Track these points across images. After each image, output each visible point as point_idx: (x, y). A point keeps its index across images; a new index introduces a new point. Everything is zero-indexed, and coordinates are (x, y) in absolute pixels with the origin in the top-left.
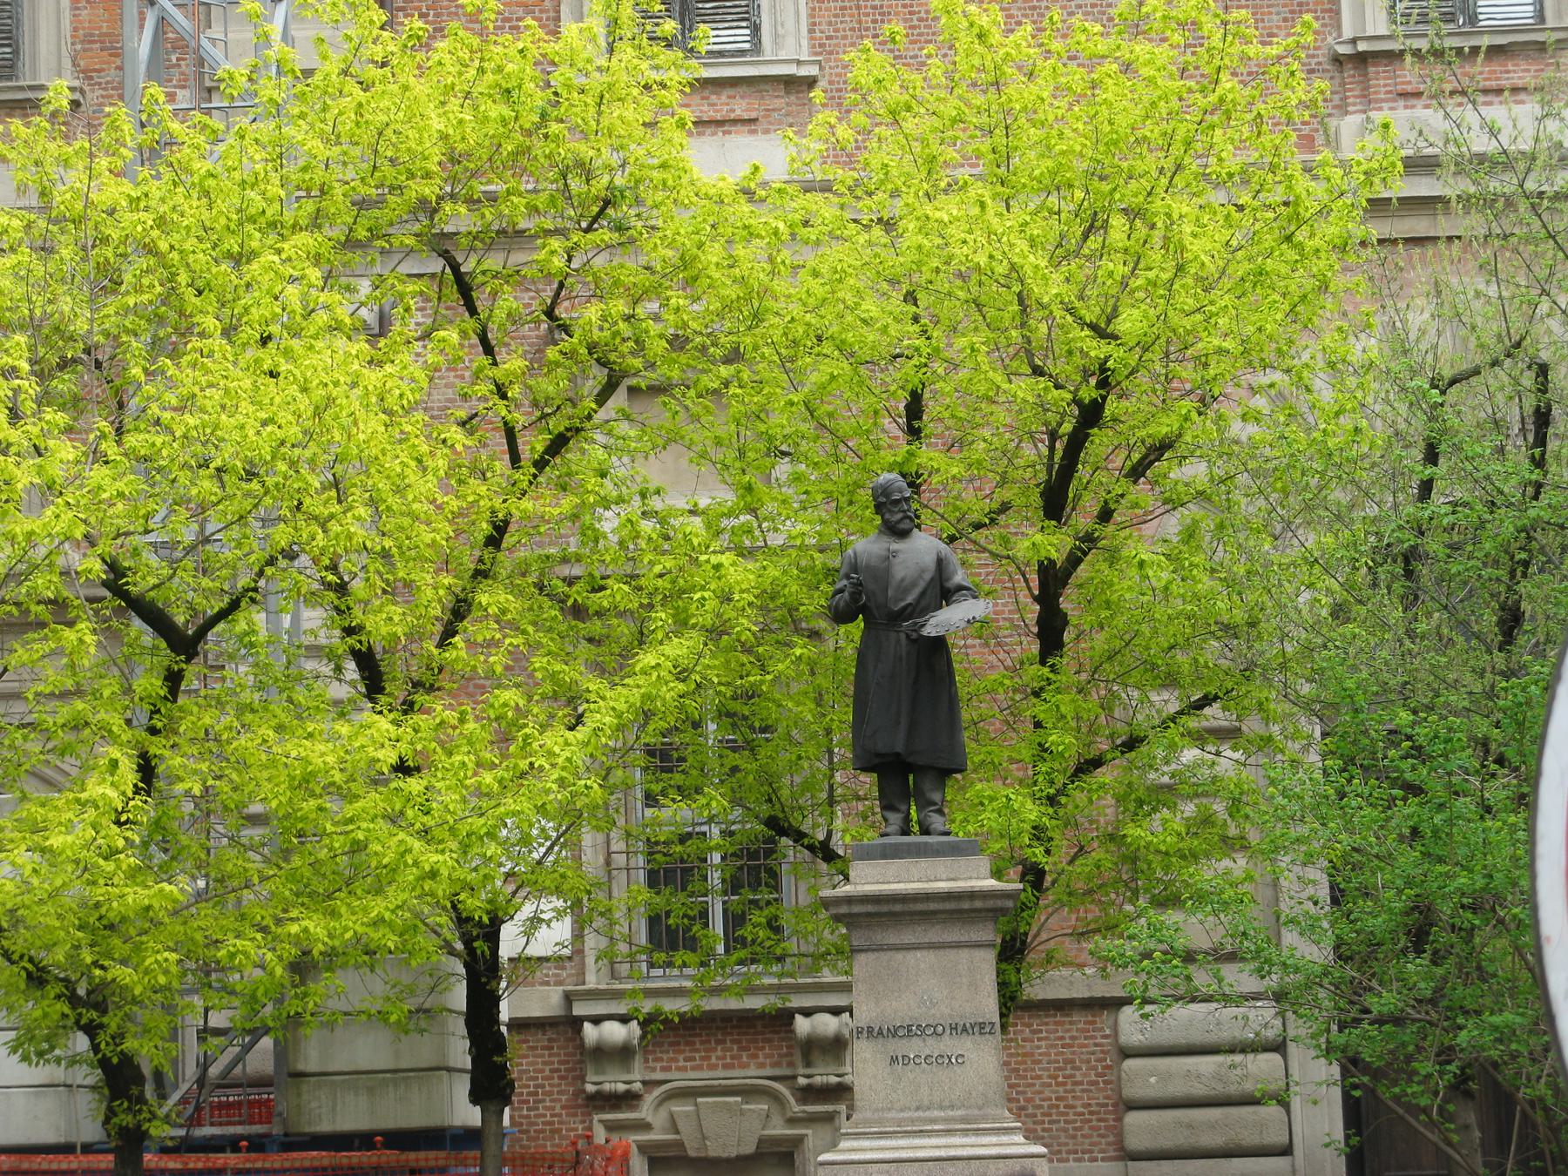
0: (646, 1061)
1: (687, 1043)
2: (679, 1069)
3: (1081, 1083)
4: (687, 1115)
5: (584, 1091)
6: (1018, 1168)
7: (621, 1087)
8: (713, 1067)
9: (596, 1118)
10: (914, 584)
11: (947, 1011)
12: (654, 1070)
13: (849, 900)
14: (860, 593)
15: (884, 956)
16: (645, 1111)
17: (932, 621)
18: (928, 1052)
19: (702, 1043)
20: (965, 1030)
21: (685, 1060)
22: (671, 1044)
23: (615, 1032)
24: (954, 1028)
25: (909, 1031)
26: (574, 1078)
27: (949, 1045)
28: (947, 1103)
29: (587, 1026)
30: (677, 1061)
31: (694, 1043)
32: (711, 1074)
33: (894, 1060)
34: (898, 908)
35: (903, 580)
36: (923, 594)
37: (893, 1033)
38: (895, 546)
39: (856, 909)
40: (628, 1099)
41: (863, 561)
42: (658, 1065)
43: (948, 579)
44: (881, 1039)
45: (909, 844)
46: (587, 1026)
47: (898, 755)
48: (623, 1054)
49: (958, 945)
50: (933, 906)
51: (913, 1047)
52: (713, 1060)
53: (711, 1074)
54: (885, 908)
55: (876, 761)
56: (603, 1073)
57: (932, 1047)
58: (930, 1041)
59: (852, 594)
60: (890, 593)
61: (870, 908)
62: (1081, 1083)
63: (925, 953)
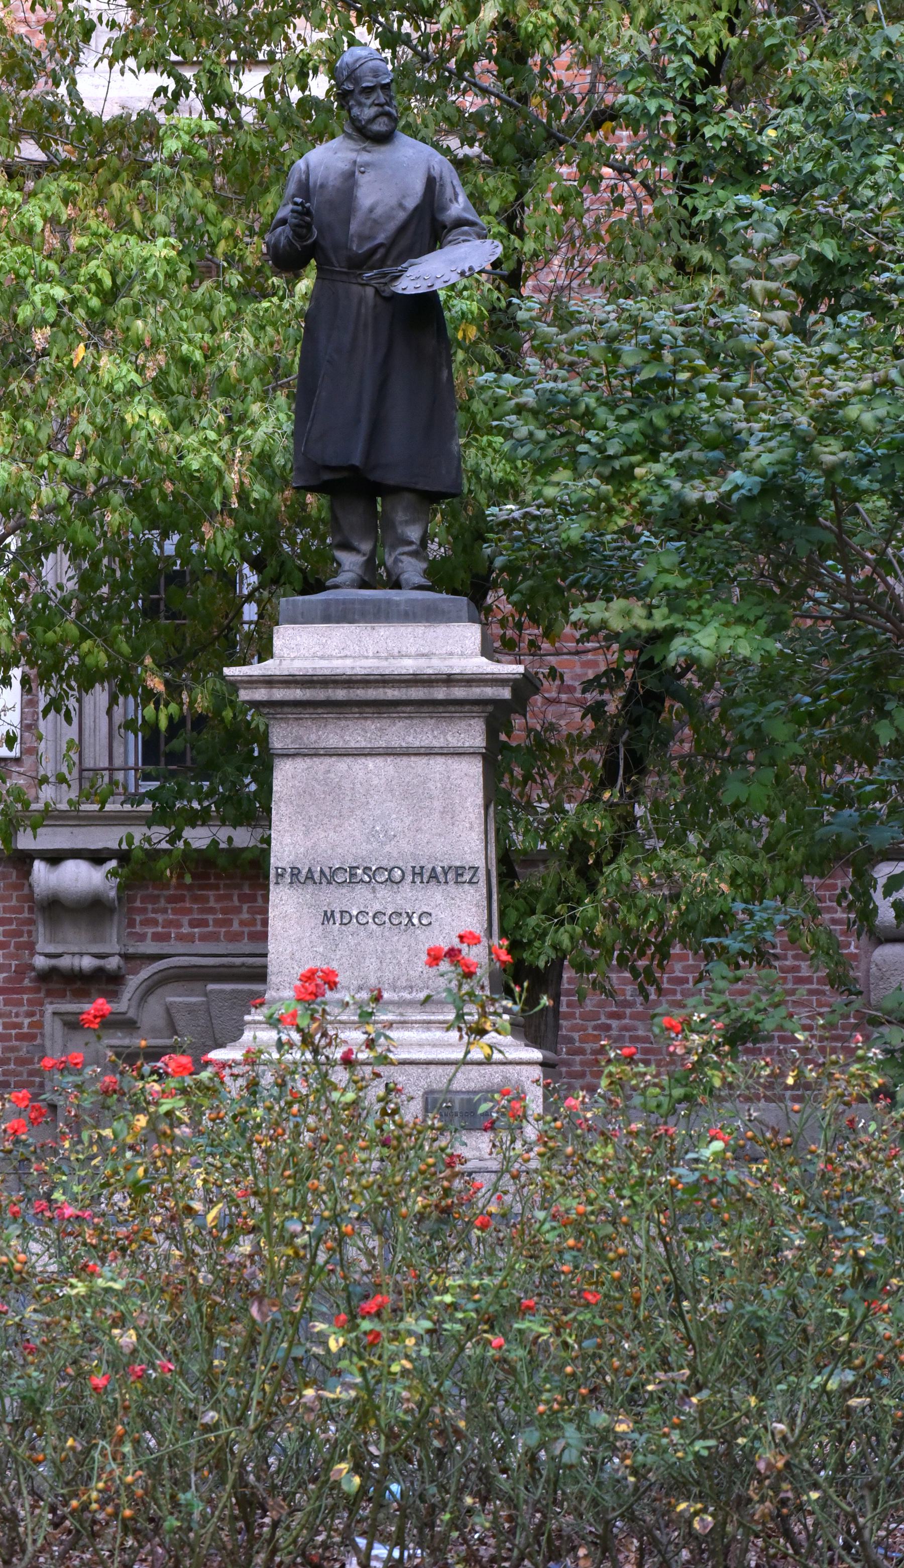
0: (131, 924)
1: (195, 899)
2: (181, 938)
3: (808, 980)
4: (191, 1009)
5: (32, 968)
6: (497, 1079)
7: (87, 963)
8: (234, 937)
9: (49, 1009)
10: (389, 217)
11: (407, 848)
12: (142, 937)
13: (269, 682)
14: (308, 226)
15: (320, 765)
16: (124, 1005)
17: (412, 272)
18: (377, 907)
19: (219, 899)
20: (433, 876)
21: (193, 924)
22: (171, 900)
23: (79, 877)
24: (417, 873)
25: (352, 876)
26: (19, 946)
27: (411, 898)
28: (403, 982)
29: (39, 867)
30: (180, 926)
31: (206, 899)
32: (232, 948)
33: (328, 917)
34: (340, 694)
35: (371, 210)
36: (402, 229)
37: (329, 877)
38: (365, 157)
39: (279, 694)
40: (105, 981)
41: (316, 178)
42: (150, 931)
43: (444, 209)
44: (311, 887)
45: (364, 602)
46: (39, 867)
47: (353, 468)
48: (92, 910)
49: (429, 753)
50: (392, 694)
51: (357, 899)
52: (236, 926)
53: (232, 948)
54: (320, 694)
55: (327, 476)
56: (64, 942)
57: (384, 899)
58: (383, 892)
59: (295, 228)
60: (354, 227)
61: (297, 694)
62: (808, 980)
63: (379, 761)
